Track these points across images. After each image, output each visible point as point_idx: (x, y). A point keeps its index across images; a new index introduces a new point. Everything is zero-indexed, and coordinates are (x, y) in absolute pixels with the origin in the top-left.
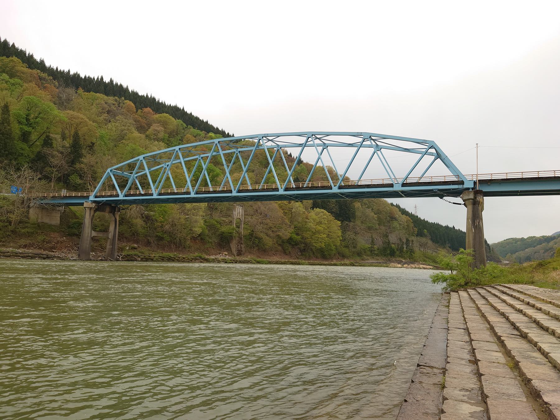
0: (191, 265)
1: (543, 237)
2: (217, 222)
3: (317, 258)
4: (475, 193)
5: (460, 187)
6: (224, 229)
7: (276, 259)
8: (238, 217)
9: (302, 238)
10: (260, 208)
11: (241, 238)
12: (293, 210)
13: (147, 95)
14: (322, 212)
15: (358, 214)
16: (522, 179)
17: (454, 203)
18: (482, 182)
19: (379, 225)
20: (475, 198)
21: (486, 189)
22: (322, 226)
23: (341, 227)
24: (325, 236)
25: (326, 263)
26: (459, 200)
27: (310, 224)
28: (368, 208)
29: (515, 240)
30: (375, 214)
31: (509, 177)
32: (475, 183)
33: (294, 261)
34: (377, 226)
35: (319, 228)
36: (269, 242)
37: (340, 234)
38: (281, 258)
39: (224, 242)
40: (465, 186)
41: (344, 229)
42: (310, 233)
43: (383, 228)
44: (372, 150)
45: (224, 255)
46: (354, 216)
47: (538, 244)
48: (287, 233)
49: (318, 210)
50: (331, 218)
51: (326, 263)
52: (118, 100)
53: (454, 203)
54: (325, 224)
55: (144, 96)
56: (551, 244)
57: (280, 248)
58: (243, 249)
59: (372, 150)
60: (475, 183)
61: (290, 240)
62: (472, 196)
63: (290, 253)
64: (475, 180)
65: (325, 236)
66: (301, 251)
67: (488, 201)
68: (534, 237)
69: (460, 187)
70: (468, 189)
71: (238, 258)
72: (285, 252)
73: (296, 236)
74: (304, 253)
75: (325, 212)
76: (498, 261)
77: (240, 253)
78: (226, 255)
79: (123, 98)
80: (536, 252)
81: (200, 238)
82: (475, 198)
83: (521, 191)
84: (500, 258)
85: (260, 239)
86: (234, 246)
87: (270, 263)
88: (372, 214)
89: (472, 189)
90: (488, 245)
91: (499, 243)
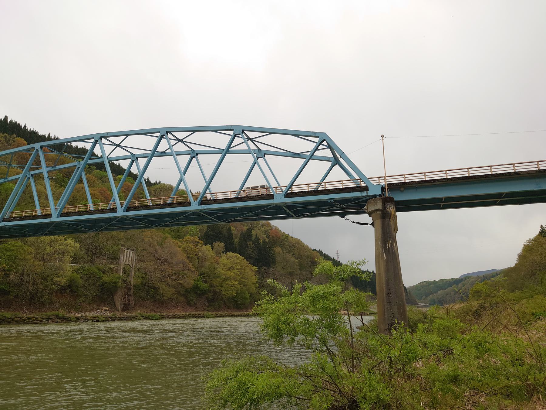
0: (41, 328)
1: (452, 279)
2: (99, 269)
3: (229, 308)
4: (387, 203)
5: (364, 194)
6: (106, 278)
7: (177, 312)
8: (127, 263)
9: (211, 286)
10: (157, 252)
11: (129, 289)
12: (200, 254)
13: (49, 135)
14: (235, 256)
15: (278, 259)
16: (447, 179)
17: (359, 223)
18: (393, 187)
19: (300, 270)
20: (384, 208)
21: (399, 197)
22: (234, 271)
23: (258, 272)
24: (237, 282)
25: (238, 313)
26: (366, 218)
27: (219, 269)
28: (289, 252)
29: (428, 283)
30: (297, 259)
31: (429, 177)
32: (383, 188)
33: (197, 313)
34: (299, 272)
35: (231, 274)
36: (167, 291)
37: (255, 279)
38: (184, 311)
39: (105, 294)
40: (370, 193)
41: (261, 275)
42: (219, 280)
43: (304, 273)
44: (250, 159)
45: (104, 312)
46: (274, 262)
47: (448, 287)
48: (190, 280)
49: (230, 254)
50: (245, 262)
51: (238, 313)
52: (8, 137)
53: (359, 223)
54: (238, 269)
55: (20, 127)
56: (460, 285)
57: (182, 298)
58: (132, 303)
59: (250, 159)
60: (383, 188)
61: (196, 290)
62: (379, 206)
63: (195, 303)
64: (382, 184)
65: (237, 282)
66: (209, 301)
67: (402, 217)
68: (444, 279)
69: (364, 194)
70: (374, 196)
71: (125, 314)
72: (189, 304)
73: (202, 284)
74: (213, 304)
75: (239, 255)
76: (415, 304)
77: (126, 307)
78: (106, 310)
79: (15, 135)
80: (447, 294)
81: (70, 290)
82: (384, 208)
83: (448, 199)
84: (417, 300)
85: (156, 289)
86: (118, 300)
87: (163, 318)
88: (293, 259)
89: (380, 196)
90: (405, 288)
91: (414, 286)
